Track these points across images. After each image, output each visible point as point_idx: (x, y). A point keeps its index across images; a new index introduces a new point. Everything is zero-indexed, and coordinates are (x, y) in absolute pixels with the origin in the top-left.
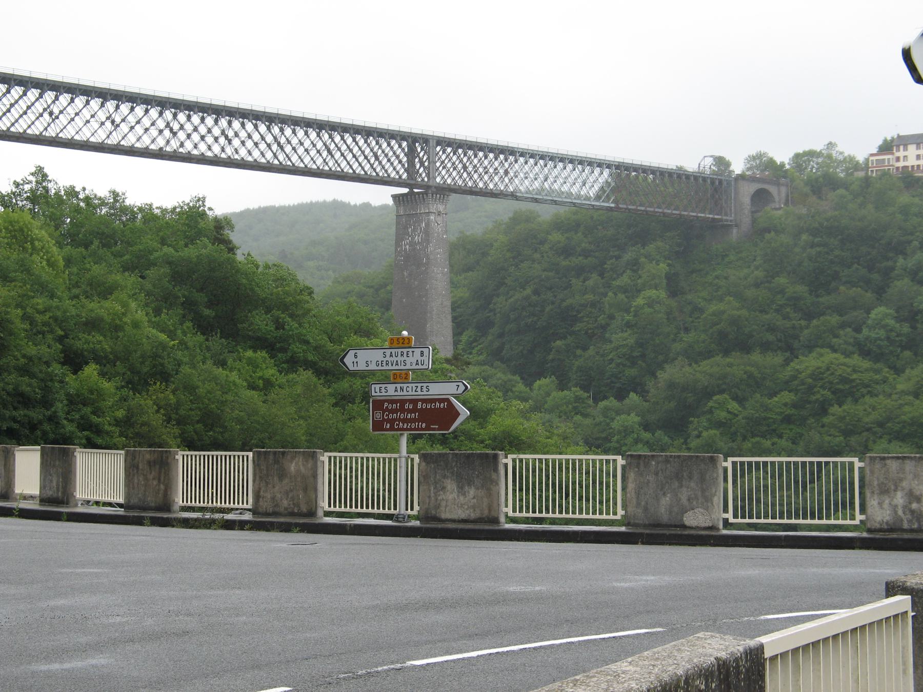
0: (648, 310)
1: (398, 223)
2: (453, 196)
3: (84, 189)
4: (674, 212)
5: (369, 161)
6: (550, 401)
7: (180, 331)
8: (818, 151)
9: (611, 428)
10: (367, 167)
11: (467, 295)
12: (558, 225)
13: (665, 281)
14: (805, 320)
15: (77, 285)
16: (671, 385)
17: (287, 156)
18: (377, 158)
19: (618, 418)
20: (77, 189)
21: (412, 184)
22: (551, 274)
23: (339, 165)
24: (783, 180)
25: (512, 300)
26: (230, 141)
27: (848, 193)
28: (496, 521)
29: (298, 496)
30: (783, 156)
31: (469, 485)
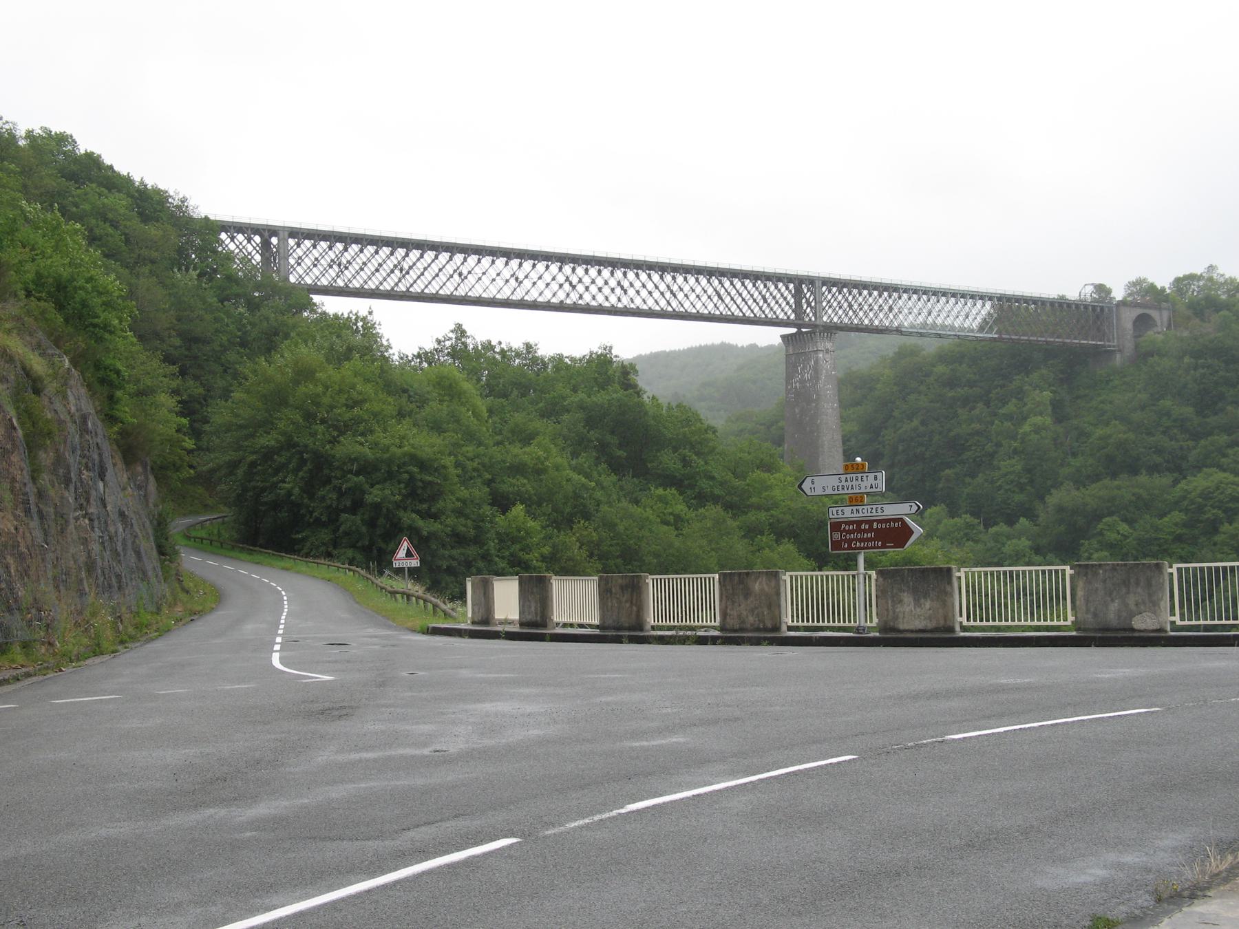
0: (1034, 437)
1: (787, 362)
2: (840, 335)
3: (500, 343)
4: (1057, 340)
5: (758, 304)
6: (941, 528)
7: (595, 473)
8: (1199, 274)
9: (1002, 553)
10: (756, 310)
11: (856, 429)
12: (942, 358)
13: (1050, 408)
14: (1193, 440)
15: (500, 433)
16: (1060, 509)
17: (680, 303)
18: (765, 301)
19: (1009, 543)
20: (493, 343)
21: (802, 324)
22: (938, 405)
23: (729, 309)
24: (1164, 305)
25: (900, 431)
26: (625, 292)
27: (1231, 314)
28: (952, 630)
29: (763, 613)
30: (1164, 281)
31: (925, 597)
